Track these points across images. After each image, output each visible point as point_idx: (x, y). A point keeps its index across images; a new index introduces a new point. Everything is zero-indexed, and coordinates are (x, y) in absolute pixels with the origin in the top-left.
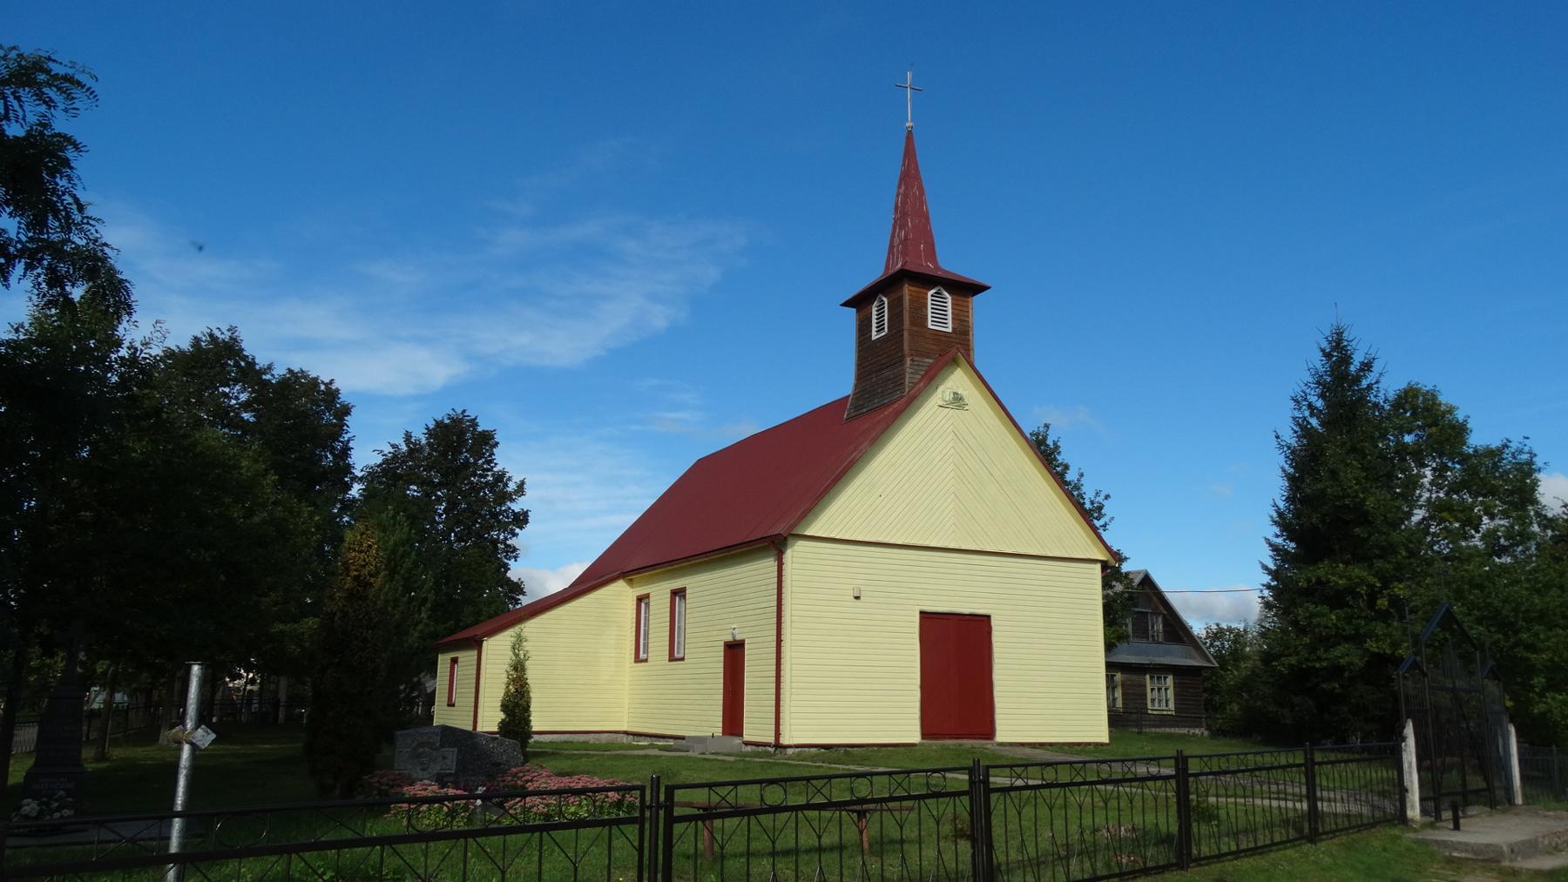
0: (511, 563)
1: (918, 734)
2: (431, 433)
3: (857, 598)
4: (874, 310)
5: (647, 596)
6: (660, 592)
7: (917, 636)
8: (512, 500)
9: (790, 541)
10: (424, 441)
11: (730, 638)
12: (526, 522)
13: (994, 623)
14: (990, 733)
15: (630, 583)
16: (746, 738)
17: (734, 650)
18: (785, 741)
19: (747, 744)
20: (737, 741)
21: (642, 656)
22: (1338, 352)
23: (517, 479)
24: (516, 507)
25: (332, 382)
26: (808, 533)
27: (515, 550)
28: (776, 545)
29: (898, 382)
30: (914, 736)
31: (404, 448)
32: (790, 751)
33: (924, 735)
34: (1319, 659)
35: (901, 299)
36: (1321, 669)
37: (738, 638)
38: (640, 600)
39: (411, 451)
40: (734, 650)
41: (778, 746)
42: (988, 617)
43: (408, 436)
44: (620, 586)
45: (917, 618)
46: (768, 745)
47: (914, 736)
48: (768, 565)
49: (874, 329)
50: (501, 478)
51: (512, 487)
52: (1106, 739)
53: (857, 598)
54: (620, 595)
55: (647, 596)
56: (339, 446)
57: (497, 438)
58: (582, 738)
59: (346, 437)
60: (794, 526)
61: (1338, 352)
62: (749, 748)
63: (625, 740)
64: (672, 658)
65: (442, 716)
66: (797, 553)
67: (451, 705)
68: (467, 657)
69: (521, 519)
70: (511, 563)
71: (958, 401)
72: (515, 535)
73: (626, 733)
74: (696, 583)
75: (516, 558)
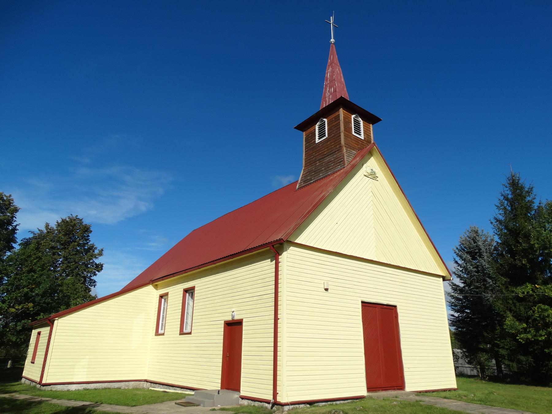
0: (92, 288)
1: (365, 388)
2: (59, 225)
3: (326, 290)
4: (317, 127)
5: (167, 294)
6: (176, 292)
7: (360, 318)
8: (95, 257)
9: (285, 245)
10: (55, 228)
11: (229, 318)
12: (102, 269)
13: (399, 311)
14: (401, 386)
15: (156, 287)
16: (243, 393)
17: (233, 328)
18: (281, 399)
19: (243, 398)
20: (236, 395)
21: (160, 331)
22: (514, 184)
23: (99, 248)
24: (97, 261)
25: (10, 196)
26: (297, 241)
27: (95, 282)
28: (274, 250)
29: (341, 161)
30: (363, 391)
31: (45, 231)
32: (286, 408)
33: (371, 388)
34: (541, 336)
35: (338, 117)
36: (541, 341)
37: (237, 318)
38: (161, 297)
39: (48, 232)
40: (233, 328)
41: (275, 403)
42: (395, 307)
43: (47, 226)
44: (150, 288)
45: (360, 306)
46: (268, 402)
47: (363, 391)
48: (267, 265)
49: (317, 137)
50: (92, 248)
51: (96, 252)
52: (455, 386)
53: (326, 290)
54: (149, 294)
55: (167, 294)
56: (10, 228)
57: (92, 229)
58: (116, 385)
59: (15, 224)
60: (290, 234)
61: (514, 184)
62: (245, 402)
63: (146, 385)
64: (182, 333)
65: (30, 371)
66: (289, 256)
67: (33, 363)
68: (45, 331)
69: (99, 267)
70: (92, 288)
71: (373, 176)
72: (95, 275)
73: (146, 381)
74: (202, 285)
75: (95, 286)
